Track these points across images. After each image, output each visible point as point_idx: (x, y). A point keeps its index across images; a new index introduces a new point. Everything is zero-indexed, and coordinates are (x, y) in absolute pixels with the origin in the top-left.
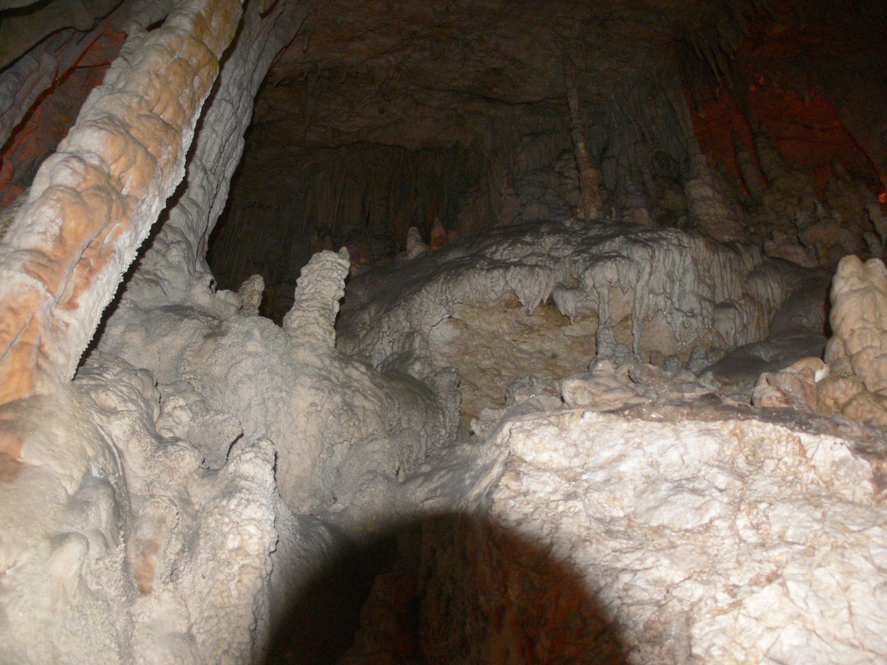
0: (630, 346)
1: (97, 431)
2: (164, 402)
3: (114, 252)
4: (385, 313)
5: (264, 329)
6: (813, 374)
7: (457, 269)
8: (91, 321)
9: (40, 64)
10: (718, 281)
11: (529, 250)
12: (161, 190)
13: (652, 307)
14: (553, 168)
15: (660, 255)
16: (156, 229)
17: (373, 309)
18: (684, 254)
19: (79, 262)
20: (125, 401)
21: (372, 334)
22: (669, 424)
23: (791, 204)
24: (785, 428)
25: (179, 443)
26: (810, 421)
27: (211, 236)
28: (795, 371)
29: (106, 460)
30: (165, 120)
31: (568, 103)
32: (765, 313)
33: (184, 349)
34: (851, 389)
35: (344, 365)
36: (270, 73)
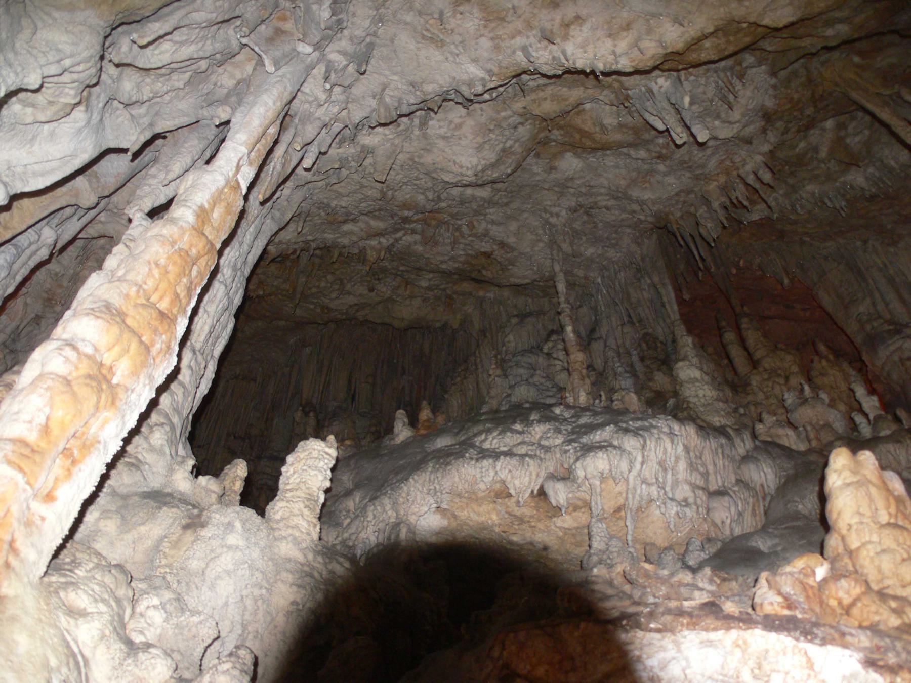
0: (624, 538)
1: (63, 636)
2: (137, 601)
3: (99, 442)
4: (370, 501)
5: (247, 520)
6: (814, 573)
7: (445, 457)
8: (69, 515)
9: (40, 236)
10: (711, 468)
11: (518, 438)
12: (151, 378)
13: (645, 498)
14: (541, 350)
15: (651, 444)
16: (144, 417)
17: (358, 496)
18: (676, 441)
19: (62, 453)
20: (96, 601)
21: (357, 522)
22: (669, 635)
23: (778, 383)
24: (790, 639)
25: (151, 650)
26: (815, 630)
27: (194, 416)
28: (795, 570)
29: (69, 670)
30: (161, 308)
31: (555, 287)
32: (760, 498)
33: (161, 539)
34: (855, 588)
35: (327, 560)
36: (265, 251)
